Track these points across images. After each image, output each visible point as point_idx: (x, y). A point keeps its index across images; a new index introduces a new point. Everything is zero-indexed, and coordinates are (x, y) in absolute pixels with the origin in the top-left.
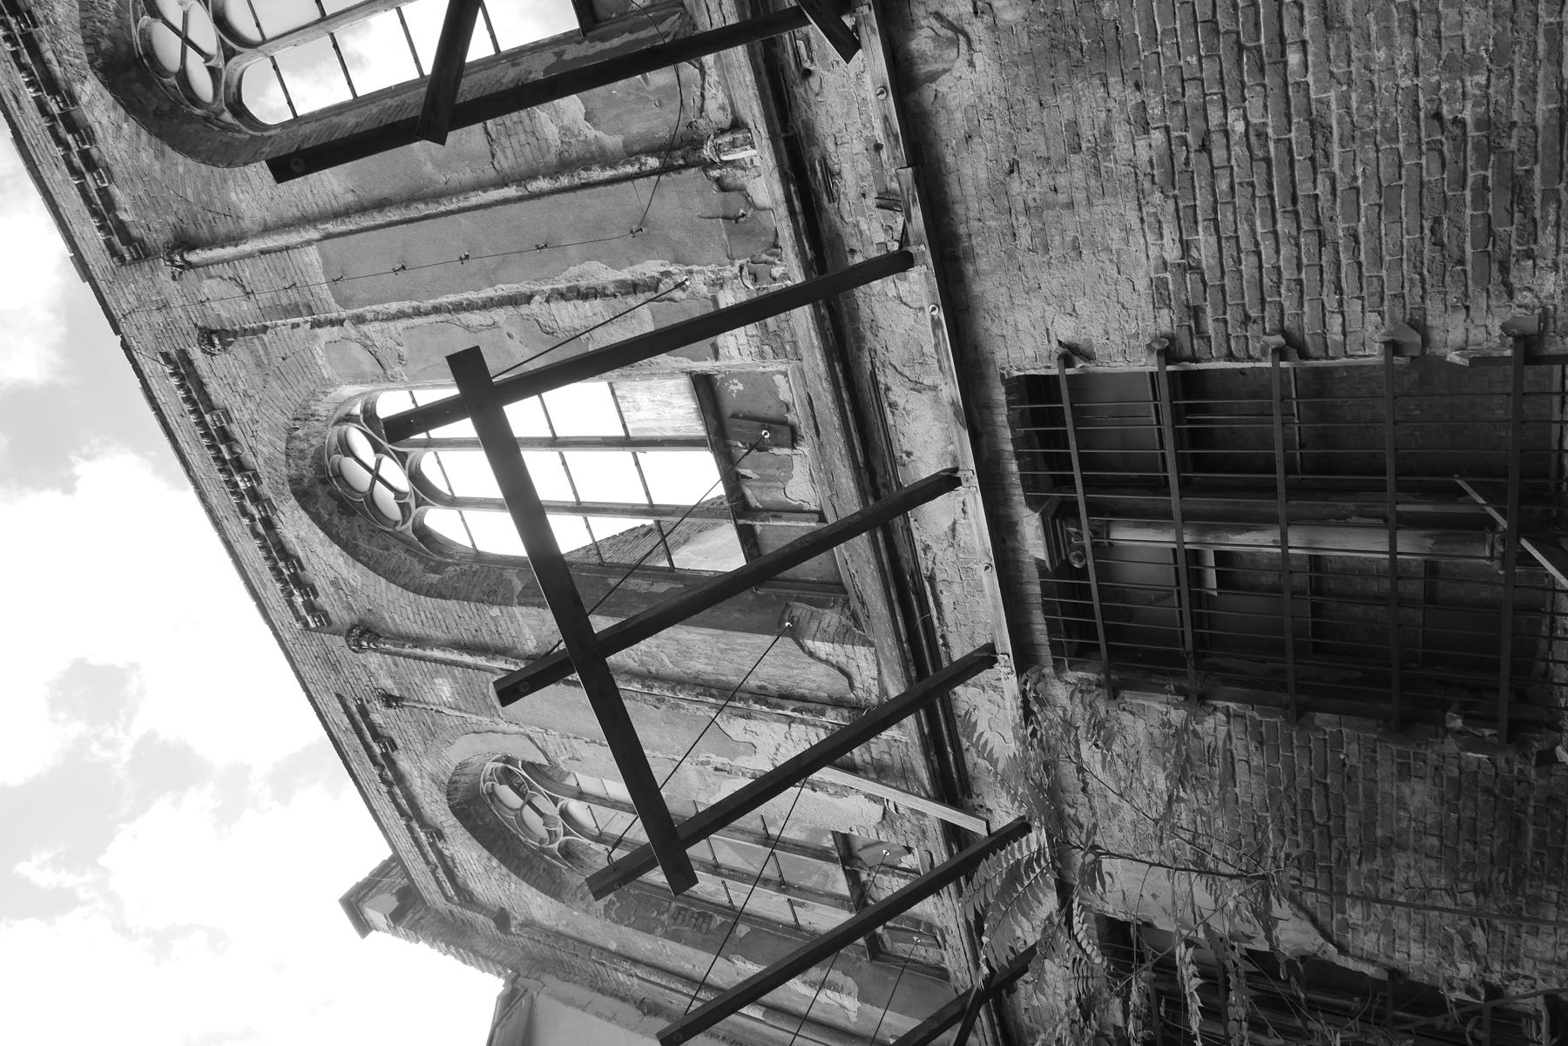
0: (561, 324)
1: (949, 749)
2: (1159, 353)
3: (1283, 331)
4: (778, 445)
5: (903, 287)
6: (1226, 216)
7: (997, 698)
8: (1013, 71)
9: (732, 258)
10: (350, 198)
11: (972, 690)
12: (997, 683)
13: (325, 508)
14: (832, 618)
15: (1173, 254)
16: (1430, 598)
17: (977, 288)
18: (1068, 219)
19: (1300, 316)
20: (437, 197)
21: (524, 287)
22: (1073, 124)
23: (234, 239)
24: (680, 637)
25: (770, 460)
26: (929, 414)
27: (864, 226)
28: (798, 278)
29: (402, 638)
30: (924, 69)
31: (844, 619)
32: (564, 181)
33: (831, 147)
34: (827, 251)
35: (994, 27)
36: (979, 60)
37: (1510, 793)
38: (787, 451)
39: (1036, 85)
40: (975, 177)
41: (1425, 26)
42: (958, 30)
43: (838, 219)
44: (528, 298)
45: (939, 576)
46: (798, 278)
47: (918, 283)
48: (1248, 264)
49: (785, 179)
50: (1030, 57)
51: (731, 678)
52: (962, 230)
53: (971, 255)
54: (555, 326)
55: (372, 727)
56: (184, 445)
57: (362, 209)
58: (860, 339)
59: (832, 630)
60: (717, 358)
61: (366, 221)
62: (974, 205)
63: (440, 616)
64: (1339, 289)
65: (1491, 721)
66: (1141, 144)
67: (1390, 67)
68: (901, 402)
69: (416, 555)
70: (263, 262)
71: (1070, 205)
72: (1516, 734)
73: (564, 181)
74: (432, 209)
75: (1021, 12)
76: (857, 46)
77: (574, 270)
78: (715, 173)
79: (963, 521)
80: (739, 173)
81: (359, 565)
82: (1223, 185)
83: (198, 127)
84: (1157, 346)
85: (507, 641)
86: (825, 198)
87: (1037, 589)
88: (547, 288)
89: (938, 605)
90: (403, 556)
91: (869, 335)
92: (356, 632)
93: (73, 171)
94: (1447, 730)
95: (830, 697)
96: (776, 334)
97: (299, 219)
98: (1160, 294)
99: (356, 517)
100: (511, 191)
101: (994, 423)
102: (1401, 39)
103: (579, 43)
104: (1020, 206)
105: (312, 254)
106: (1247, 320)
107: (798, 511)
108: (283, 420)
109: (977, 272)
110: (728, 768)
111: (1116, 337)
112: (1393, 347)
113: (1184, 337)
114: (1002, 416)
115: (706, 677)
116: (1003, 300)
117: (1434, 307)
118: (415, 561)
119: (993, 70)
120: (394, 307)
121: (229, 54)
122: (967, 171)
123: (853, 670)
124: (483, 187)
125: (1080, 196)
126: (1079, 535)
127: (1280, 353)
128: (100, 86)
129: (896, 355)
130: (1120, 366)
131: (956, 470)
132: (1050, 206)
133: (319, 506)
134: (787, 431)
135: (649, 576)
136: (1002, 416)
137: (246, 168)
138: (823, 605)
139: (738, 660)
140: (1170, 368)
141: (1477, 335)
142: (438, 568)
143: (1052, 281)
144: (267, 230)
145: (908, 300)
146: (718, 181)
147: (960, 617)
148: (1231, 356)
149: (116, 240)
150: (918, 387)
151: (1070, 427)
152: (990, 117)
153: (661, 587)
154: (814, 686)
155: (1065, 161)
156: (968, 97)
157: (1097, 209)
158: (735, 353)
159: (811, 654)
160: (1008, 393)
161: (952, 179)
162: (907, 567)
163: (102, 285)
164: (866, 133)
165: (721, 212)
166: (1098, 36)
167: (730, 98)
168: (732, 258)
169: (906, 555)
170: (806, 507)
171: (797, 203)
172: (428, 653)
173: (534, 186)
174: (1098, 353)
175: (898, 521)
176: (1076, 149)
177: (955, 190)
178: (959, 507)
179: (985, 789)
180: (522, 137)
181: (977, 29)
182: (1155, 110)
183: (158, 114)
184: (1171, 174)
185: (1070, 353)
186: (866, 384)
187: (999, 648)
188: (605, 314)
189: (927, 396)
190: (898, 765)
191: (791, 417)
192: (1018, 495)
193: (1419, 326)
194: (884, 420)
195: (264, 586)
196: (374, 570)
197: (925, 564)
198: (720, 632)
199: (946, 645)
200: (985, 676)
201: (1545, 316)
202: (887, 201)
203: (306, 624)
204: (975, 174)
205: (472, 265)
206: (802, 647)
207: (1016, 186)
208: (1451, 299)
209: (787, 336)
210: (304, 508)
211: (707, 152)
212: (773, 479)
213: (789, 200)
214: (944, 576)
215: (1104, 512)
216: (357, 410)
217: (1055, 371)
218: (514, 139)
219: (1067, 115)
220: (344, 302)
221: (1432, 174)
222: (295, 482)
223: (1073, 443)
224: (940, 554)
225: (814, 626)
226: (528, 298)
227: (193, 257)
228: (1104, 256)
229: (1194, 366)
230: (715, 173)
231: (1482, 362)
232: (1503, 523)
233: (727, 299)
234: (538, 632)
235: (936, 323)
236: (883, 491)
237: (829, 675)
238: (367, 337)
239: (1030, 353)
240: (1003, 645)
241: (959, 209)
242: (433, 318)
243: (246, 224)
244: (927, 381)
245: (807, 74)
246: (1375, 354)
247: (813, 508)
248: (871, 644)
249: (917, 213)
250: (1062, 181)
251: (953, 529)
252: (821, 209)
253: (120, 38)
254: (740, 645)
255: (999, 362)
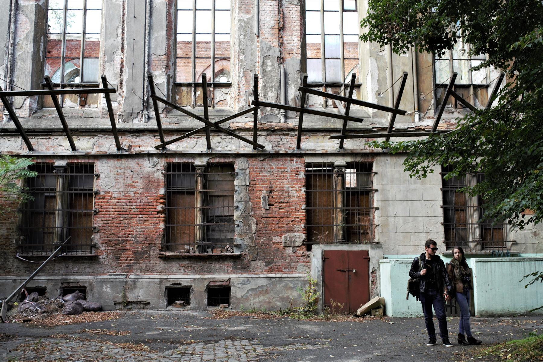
0: (116, 57)
3: (99, 212)
4: (80, 101)
6: (119, 204)
7: (19, 148)
8: (147, 174)
9: (124, 111)
11: (20, 142)
14: (35, 106)
15: (114, 195)
16: (44, 233)
17: (112, 160)
18: (122, 179)
19: (101, 214)
20: (149, 35)
21: (125, 52)
22: (137, 182)
26: (88, 146)
27: (126, 141)
30: (151, 159)
31: (35, 109)
33: (142, 138)
34: (122, 133)
35: (155, 172)
36: (150, 168)
37: (6, 247)
38: (79, 103)
39: (144, 177)
40: (131, 164)
41: (142, 233)
42: (155, 166)
44: (123, 52)
47: (113, 150)
48: (111, 207)
49: (137, 129)
50: (149, 177)
52: (123, 160)
53: (118, 160)
57: (151, 8)
58: (105, 135)
59: (32, 106)
62: (127, 163)
64: (105, 220)
65: (22, 243)
66: (132, 193)
68: (91, 140)
71: (124, 180)
72: (20, 247)
74: (147, 34)
75: (156, 177)
76: (157, 149)
77: (127, 70)
80: (140, 117)
82: (124, 204)
89: (43, 139)
91: (105, 137)
94: (20, 236)
95: (13, 102)
100: (146, 60)
101: (85, 159)
102: (140, 230)
107: (63, 101)
112: (95, 228)
113: (100, 196)
114: (86, 161)
116: (109, 165)
117: (101, 234)
120: (126, 6)
122: (133, 163)
123: (21, 110)
124: (149, 52)
125: (125, 182)
126: (60, 172)
127: (95, 211)
129: (100, 141)
130: (95, 184)
132: (125, 176)
134: (84, 105)
136: (86, 161)
138: (38, 103)
141: (96, 239)
143: (112, 174)
145: (111, 146)
146: (139, 112)
148: (95, 203)
150: (94, 145)
156: (145, 165)
157: (123, 184)
161: (132, 160)
162: (53, 134)
165: (133, 112)
166: (150, 188)
168: (124, 111)
169: (56, 134)
170: (64, 104)
173: (146, 65)
175: (65, 134)
176: (133, 182)
177: (130, 160)
178: (67, 148)
181: (155, 169)
182: (137, 195)
184: (127, 197)
185: (98, 176)
186: (95, 134)
187: (33, 152)
189: (91, 146)
191: (87, 106)
192: (70, 161)
193: (98, 232)
194: (87, 136)
197: (53, 138)
198: (31, 74)
199: (32, 138)
201: (98, 248)
202: (130, 147)
207: (129, 171)
208: (102, 236)
211: (145, 111)
213: (133, 129)
215: (64, 178)
217: (95, 173)
219: (139, 181)
225: (33, 101)
226: (123, 52)
228: (115, 184)
229: (94, 197)
231: (92, 240)
232: (63, 244)
234: (27, 8)
235: (106, 152)
236: (71, 132)
237: (20, 103)
239: (99, 168)
241: (126, 160)
245: (155, 137)
246: (94, 225)
247: (64, 105)
248: (29, 117)
249: (127, 153)
250: (128, 179)
251: (62, 146)
252: (131, 134)
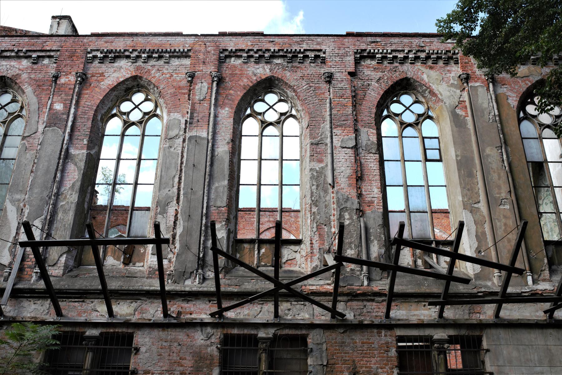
0: (169, 209)
1: (29, 295)
2: (134, 371)
5: (159, 312)
7: (45, 313)
9: (175, 270)
10: (216, 153)
11: (48, 306)
12: (49, 314)
13: (129, 83)
14: (71, 263)
17: (156, 330)
20: (209, 185)
21: (181, 203)
23: (216, 105)
25: (120, 255)
27: (175, 306)
28: (167, 288)
29: (79, 95)
30: (204, 329)
31: (70, 267)
32: (203, 228)
33: (194, 303)
35: (208, 346)
38: (122, 260)
40: (180, 335)
42: (209, 338)
43: (178, 300)
45: (84, 304)
46: (167, 288)
47: (159, 316)
51: (55, 225)
53: (163, 330)
54: (169, 207)
55: (43, 57)
56: (161, 38)
58: (150, 298)
59: (68, 263)
60: (151, 254)
61: (209, 158)
62: (174, 334)
63: (86, 116)
66: (178, 372)
68: (132, 305)
69: (107, 111)
70: (207, 112)
71: (169, 355)
73: (203, 228)
74: (206, 183)
75: (209, 352)
77: (182, 222)
78: (195, 272)
79: (99, 314)
80: (194, 278)
81: (108, 90)
83: (249, 101)
84: (135, 370)
85: (75, 142)
86: (183, 299)
87: (77, 330)
88: (179, 210)
89: (75, 302)
90: (108, 106)
91: (150, 301)
92: (84, 77)
93: (249, 50)
96: (154, 273)
97: (215, 131)
99: (124, 92)
100: (204, 211)
101: (123, 328)
103: (233, 238)
104: (171, 344)
105: (204, 135)
108: (162, 86)
109: (159, 331)
110: (23, 214)
114: (125, 330)
115: (56, 216)
116: (152, 336)
118: (105, 111)
119: (199, 344)
120: (185, 155)
121: (263, 122)
122: (181, 334)
123: (55, 268)
124: (208, 203)
125: (171, 358)
126: (91, 344)
128: (267, 76)
129: (144, 306)
130: (132, 361)
131: (113, 317)
132: (170, 351)
133: (131, 82)
134: (127, 263)
135: (90, 201)
136: (125, 330)
137: (232, 119)
138: (75, 260)
140: (130, 372)
142: (102, 119)
143: (154, 348)
144: (216, 116)
146: (193, 272)
147: (71, 307)
149: (227, 53)
150: (135, 310)
151: (120, 347)
152: (191, 341)
153: (102, 262)
154: (51, 253)
155: (179, 356)
157: (167, 361)
158: (152, 260)
159: (61, 255)
160: (130, 333)
161: (180, 330)
162: (88, 296)
163: (216, 39)
164: (195, 312)
165: (186, 271)
167: (210, 279)
169: (91, 296)
171: (184, 293)
172: (73, 107)
173: (204, 218)
174: (136, 356)
176: (180, 359)
178: (103, 314)
179: (13, 302)
180: (216, 217)
183: (255, 90)
185: (137, 350)
186: (138, 297)
187: (62, 318)
188: (169, 224)
189: (132, 312)
190: (23, 276)
191: (131, 264)
192: (104, 330)
194: (128, 299)
195: (106, 42)
196: (105, 96)
197: (88, 301)
198: (71, 227)
199: (63, 301)
200: (53, 310)
202: (179, 313)
203: (89, 53)
204: (180, 335)
205: (190, 191)
206: (64, 253)
207: (176, 344)
209: (153, 276)
210: (131, 77)
211: (200, 271)
212: (115, 254)
214: (84, 305)
216: (158, 112)
217: (133, 346)
218: (216, 214)
219: (187, 358)
220: (191, 138)
222: (141, 78)
223: (116, 347)
224: (90, 305)
225: (70, 257)
227: (215, 84)
228: (157, 361)
230: (195, 272)
233: (165, 262)
234: (77, 157)
235: (150, 320)
236: (110, 294)
237: (54, 259)
238: (179, 138)
240: (63, 319)
241: (174, 330)
242: (179, 168)
243: (219, 110)
244: (136, 313)
245: (210, 301)
248: (63, 275)
249: (175, 321)
250: (175, 354)
251: (97, 311)
253: (276, 86)
254: (66, 232)
255: (138, 332)
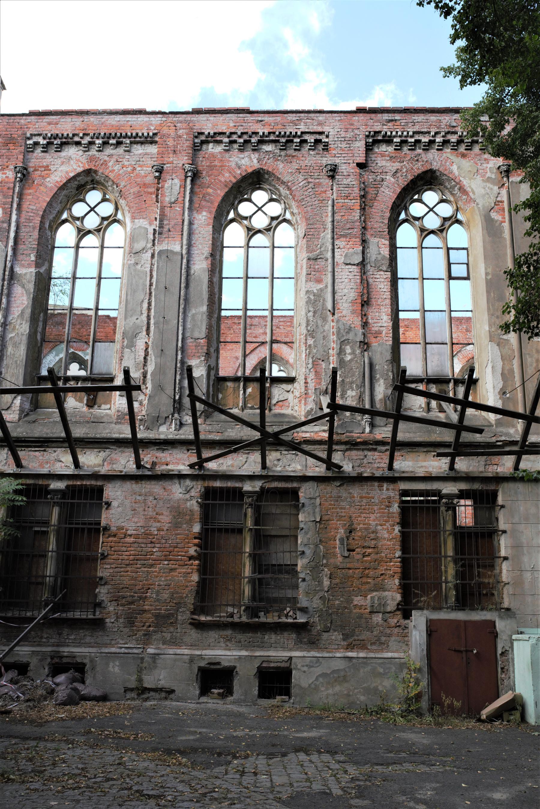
3: (108, 555)
5: (131, 463)
9: (147, 415)
14: (27, 406)
15: (129, 532)
18: (141, 509)
20: (185, 312)
21: (152, 334)
22: (162, 514)
23: (190, 209)
24: (22, 345)
30: (182, 481)
32: (179, 365)
33: (170, 452)
35: (187, 500)
40: (155, 488)
41: (167, 587)
42: (188, 492)
44: (148, 334)
45: (45, 453)
47: (131, 467)
48: (124, 549)
52: (143, 482)
53: (137, 483)
58: (120, 447)
59: (23, 406)
62: (149, 487)
63: (31, 224)
66: (155, 529)
67: (160, 580)
68: (100, 454)
69: (56, 216)
71: (144, 510)
73: (179, 365)
74: (181, 310)
77: (153, 358)
82: (143, 546)
85: (20, 257)
89: (36, 451)
91: (120, 450)
96: (124, 418)
98: (120, 528)
102: (165, 583)
106: (111, 547)
111: (111, 516)
113: (109, 532)
114: (93, 483)
116: (124, 489)
117: (109, 587)
118: (54, 215)
120: (155, 274)
122: (157, 487)
124: (183, 334)
125: (146, 513)
126: (57, 498)
127: (102, 554)
129: (113, 456)
130: (104, 516)
132: (145, 505)
137: (211, 226)
139: (13, 367)
141: (102, 595)
142: (50, 227)
143: (127, 502)
144: (191, 223)
148: (103, 543)
150: (104, 460)
156: (174, 491)
158: (120, 402)
162: (49, 444)
169: (53, 445)
172: (14, 212)
173: (179, 353)
176: (157, 514)
180: (194, 351)
181: (188, 496)
183: (239, 187)
184: (147, 534)
185: (108, 504)
186: (107, 446)
187: (22, 469)
192: (71, 483)
193: (105, 584)
197: (50, 450)
201: (105, 608)
202: (154, 464)
203: (29, 139)
205: (162, 319)
207: (151, 498)
209: (123, 421)
210: (84, 171)
211: (176, 415)
217: (104, 500)
219: (165, 513)
221: (137, 587)
222: (96, 172)
226: (148, 334)
229: (101, 534)
231: (96, 596)
233: (136, 405)
235: (121, 472)
241: (148, 483)
245: (188, 450)
246: (100, 574)
248: (19, 421)
250: (150, 509)
251: (61, 461)
253: (266, 181)
